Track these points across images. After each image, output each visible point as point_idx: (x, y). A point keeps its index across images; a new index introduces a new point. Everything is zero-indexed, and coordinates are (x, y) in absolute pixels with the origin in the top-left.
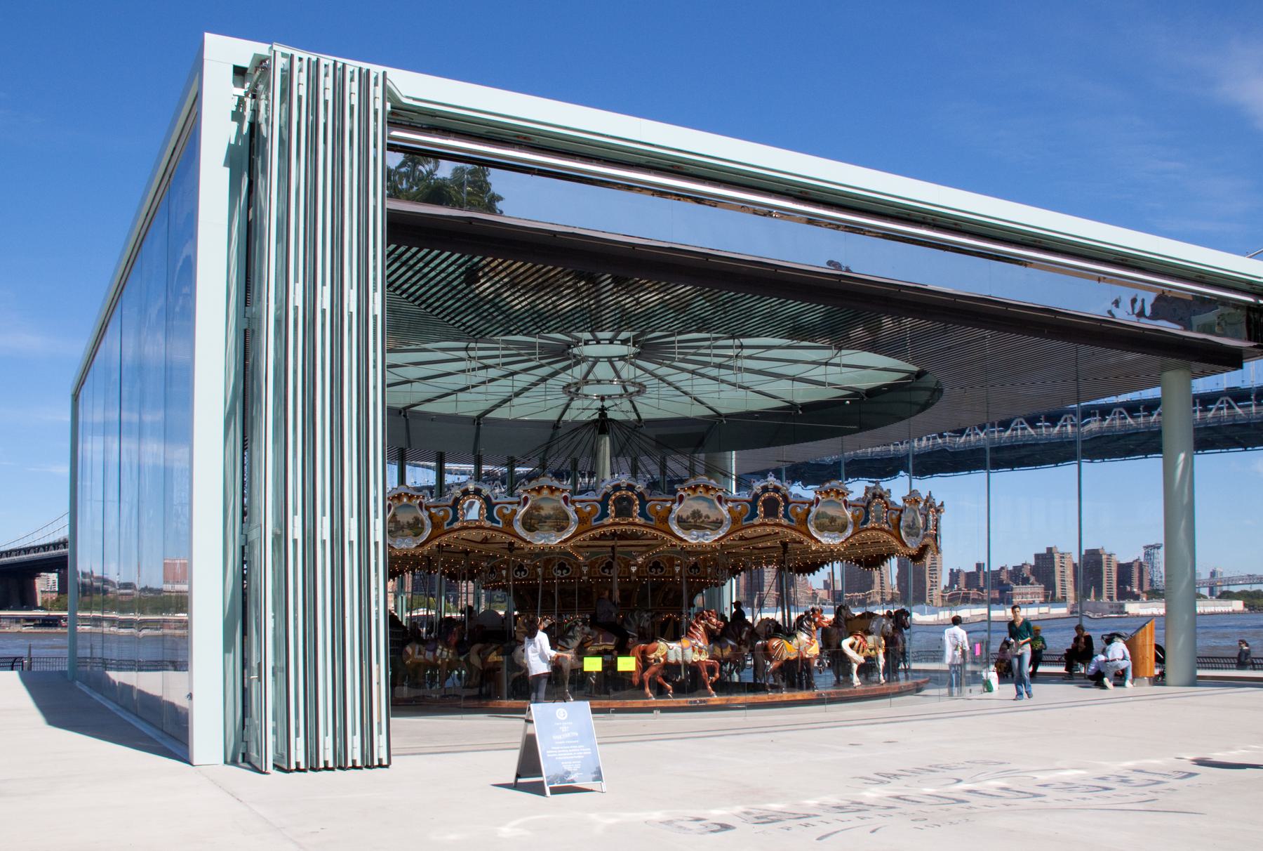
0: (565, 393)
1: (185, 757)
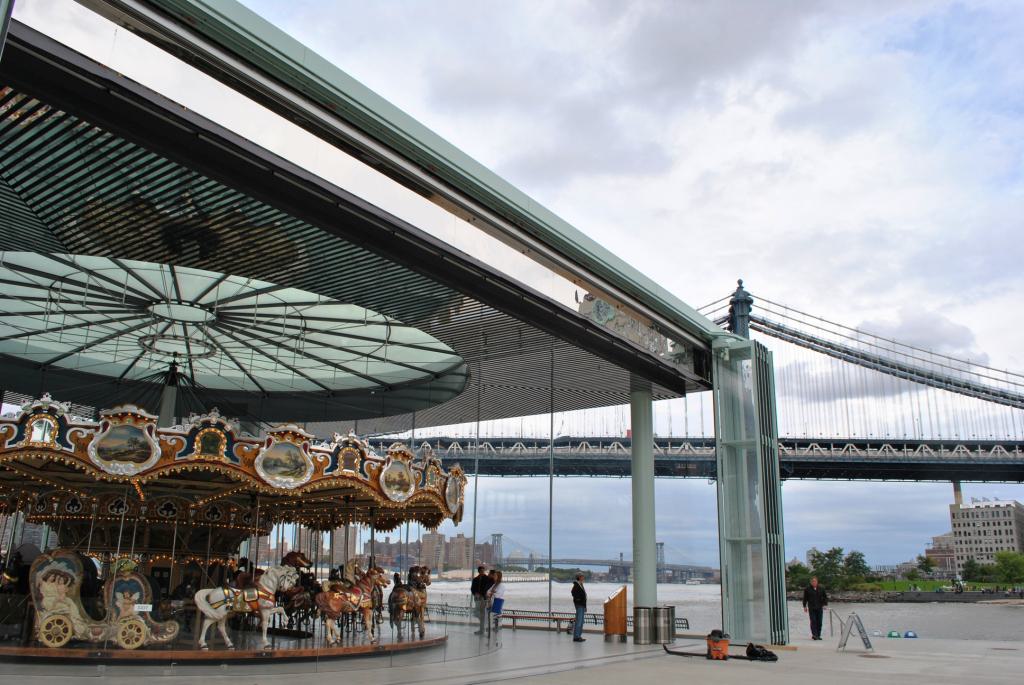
0: (139, 345)
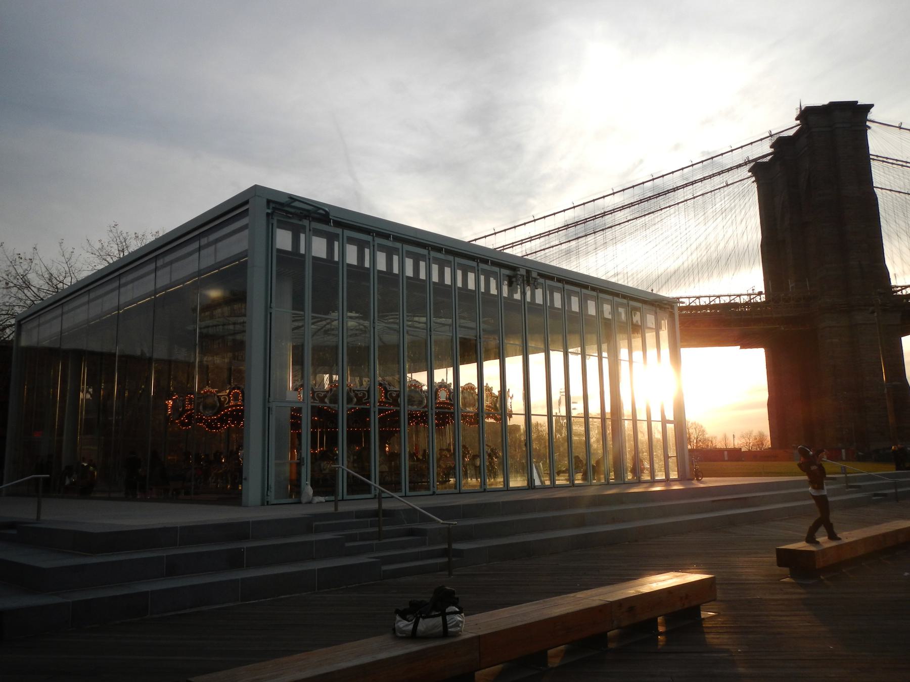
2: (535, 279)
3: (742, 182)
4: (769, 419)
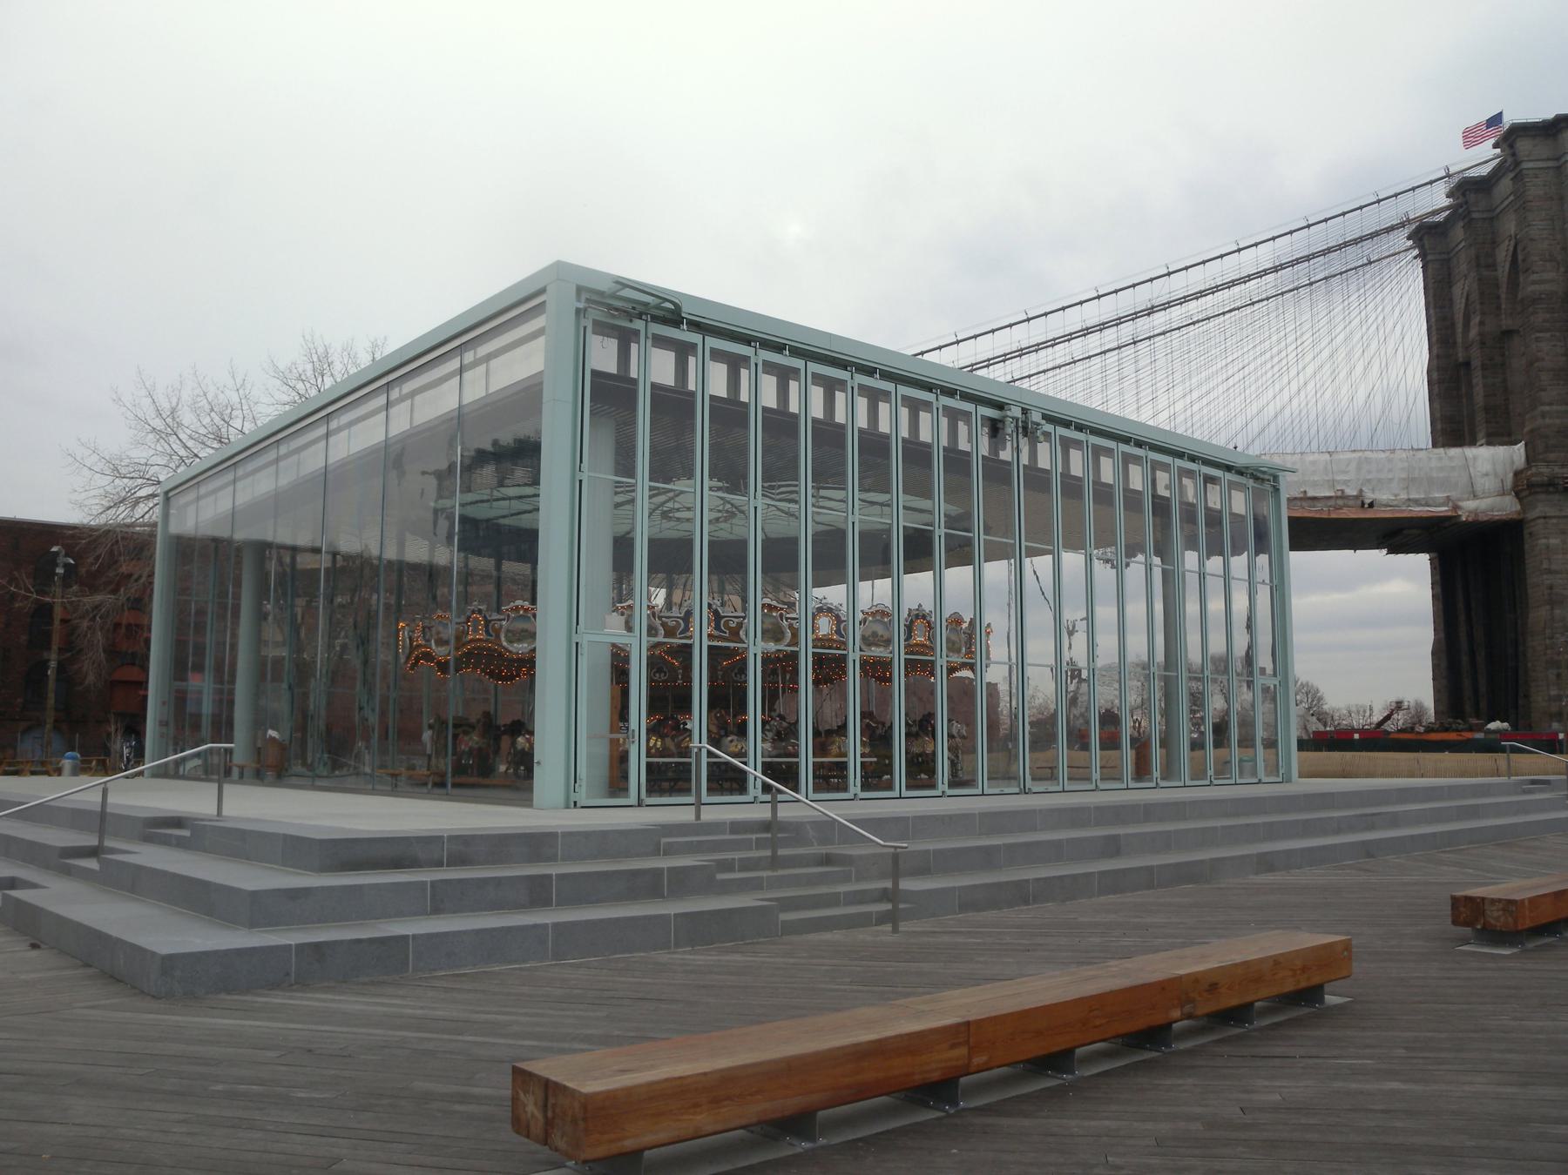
1: (1501, 113)
2: (1038, 424)
3: (1397, 257)
4: (1434, 679)
